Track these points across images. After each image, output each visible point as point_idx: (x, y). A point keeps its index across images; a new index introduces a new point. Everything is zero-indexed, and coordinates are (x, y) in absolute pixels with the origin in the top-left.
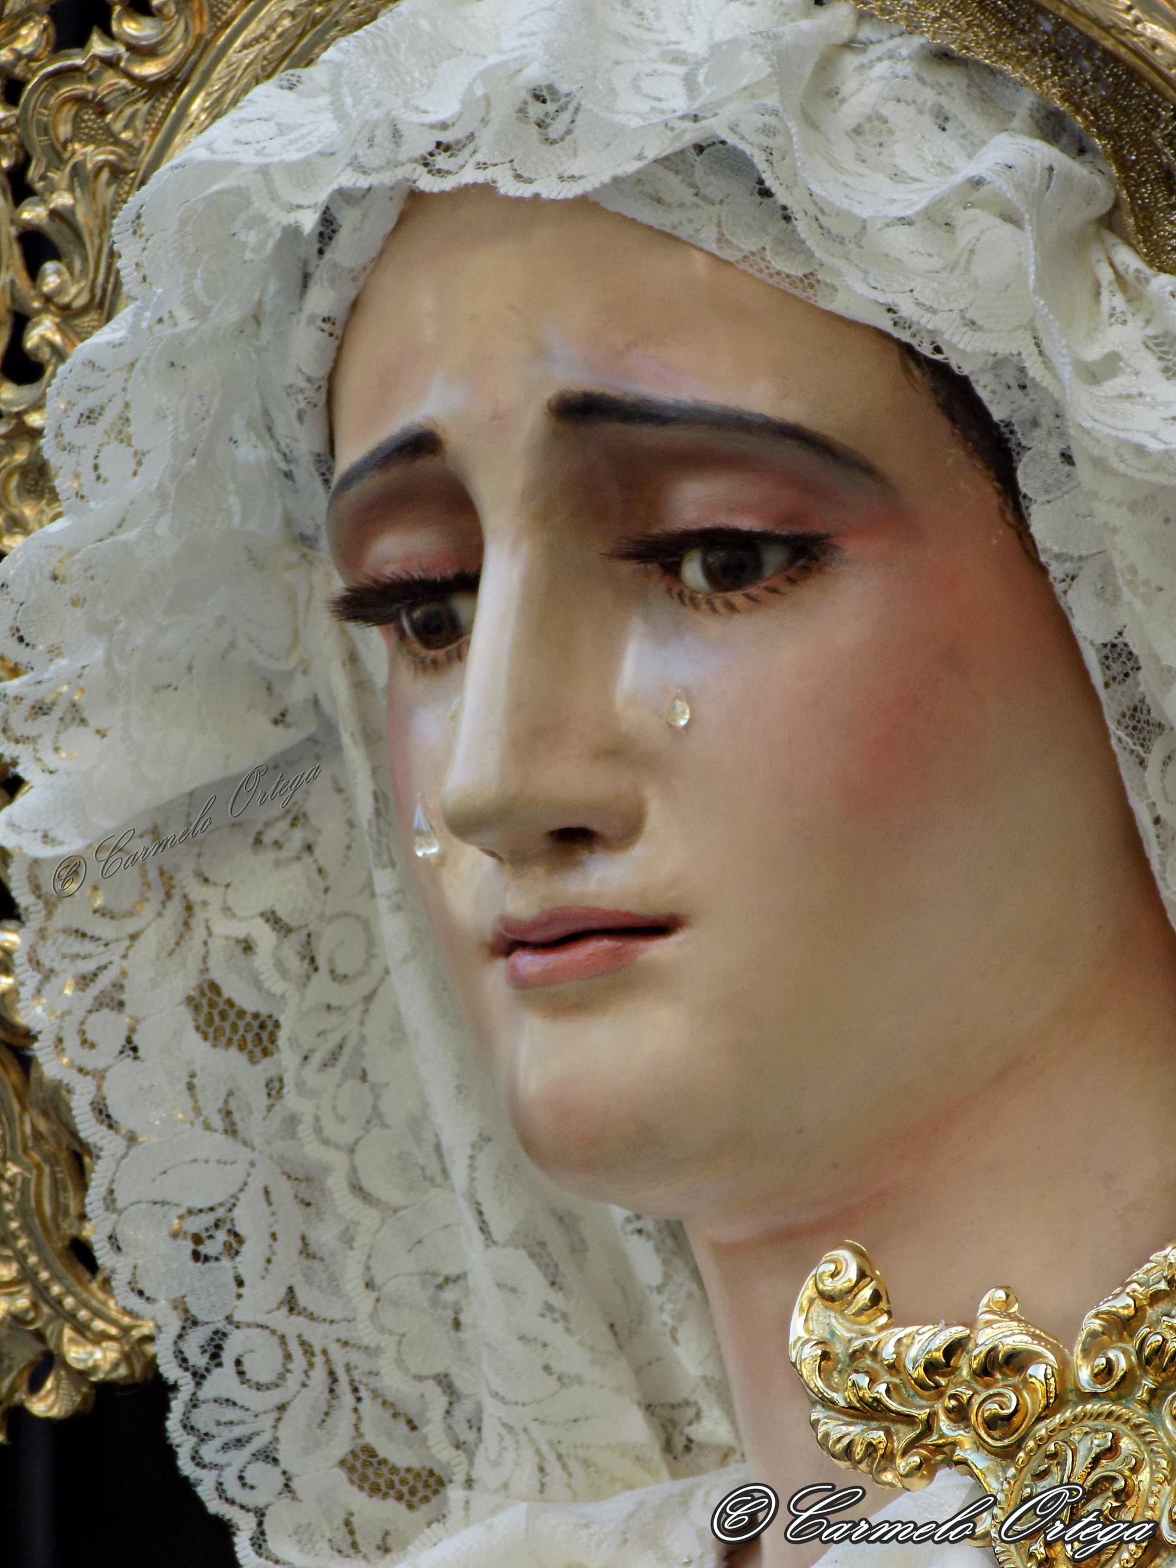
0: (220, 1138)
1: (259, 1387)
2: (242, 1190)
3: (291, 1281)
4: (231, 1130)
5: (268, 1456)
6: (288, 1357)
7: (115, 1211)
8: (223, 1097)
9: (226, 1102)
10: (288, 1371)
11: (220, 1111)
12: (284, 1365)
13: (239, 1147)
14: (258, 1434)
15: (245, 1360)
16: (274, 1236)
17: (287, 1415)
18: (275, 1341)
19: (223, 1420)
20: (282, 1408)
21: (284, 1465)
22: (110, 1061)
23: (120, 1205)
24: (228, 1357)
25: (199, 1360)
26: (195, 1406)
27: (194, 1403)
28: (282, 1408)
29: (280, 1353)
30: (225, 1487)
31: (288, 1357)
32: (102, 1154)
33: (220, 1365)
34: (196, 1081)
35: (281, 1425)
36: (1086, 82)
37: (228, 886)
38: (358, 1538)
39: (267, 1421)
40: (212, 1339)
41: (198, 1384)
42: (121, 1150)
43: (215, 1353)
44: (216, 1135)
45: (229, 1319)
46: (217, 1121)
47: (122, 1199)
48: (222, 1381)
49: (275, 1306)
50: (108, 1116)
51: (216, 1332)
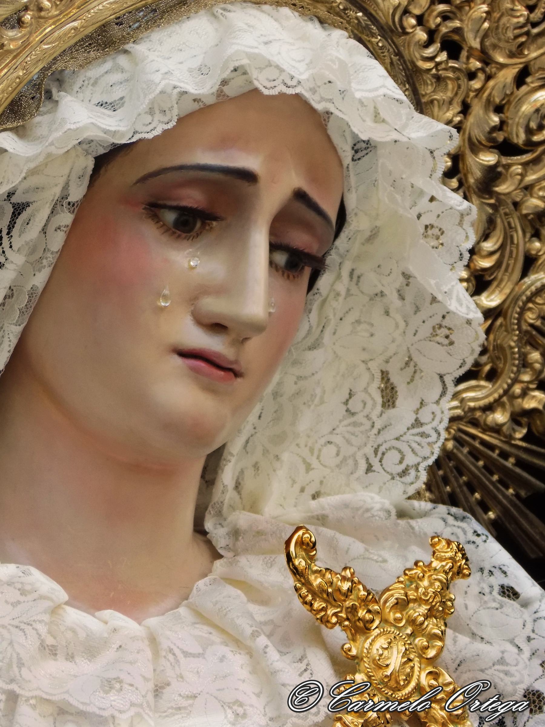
0: (415, 359)
1: (400, 451)
2: (421, 340)
3: (429, 305)
4: (410, 358)
5: (418, 423)
6: (383, 454)
7: (464, 361)
8: (405, 370)
9: (405, 368)
10: (386, 449)
11: (409, 366)
12: (387, 452)
13: (411, 352)
14: (413, 435)
15: (398, 462)
16: (424, 322)
17: (398, 435)
18: (384, 462)
19: (420, 447)
20: (397, 439)
21: (414, 417)
22: (431, 404)
23: (462, 361)
24: (403, 467)
25: (413, 472)
26: (425, 458)
27: (425, 458)
28: (397, 439)
29: (385, 457)
30: (460, 365)
31: (383, 454)
32: (454, 379)
33: (408, 466)
34: (409, 381)
35: (402, 433)
36: (118, 43)
37: (390, 334)
38: (412, 374)
39: (408, 437)
40: (404, 476)
41: (419, 464)
42: (447, 375)
43: (404, 473)
44: (415, 361)
45: (393, 478)
46: (412, 364)
47: (460, 362)
48: (411, 460)
49: (375, 473)
50: (443, 388)
51: (401, 477)
